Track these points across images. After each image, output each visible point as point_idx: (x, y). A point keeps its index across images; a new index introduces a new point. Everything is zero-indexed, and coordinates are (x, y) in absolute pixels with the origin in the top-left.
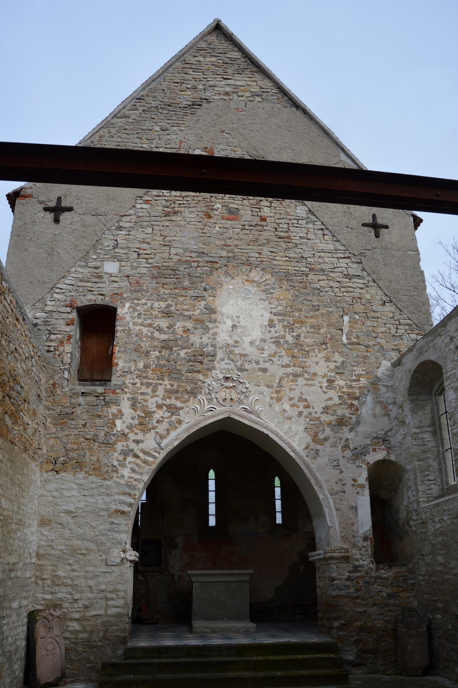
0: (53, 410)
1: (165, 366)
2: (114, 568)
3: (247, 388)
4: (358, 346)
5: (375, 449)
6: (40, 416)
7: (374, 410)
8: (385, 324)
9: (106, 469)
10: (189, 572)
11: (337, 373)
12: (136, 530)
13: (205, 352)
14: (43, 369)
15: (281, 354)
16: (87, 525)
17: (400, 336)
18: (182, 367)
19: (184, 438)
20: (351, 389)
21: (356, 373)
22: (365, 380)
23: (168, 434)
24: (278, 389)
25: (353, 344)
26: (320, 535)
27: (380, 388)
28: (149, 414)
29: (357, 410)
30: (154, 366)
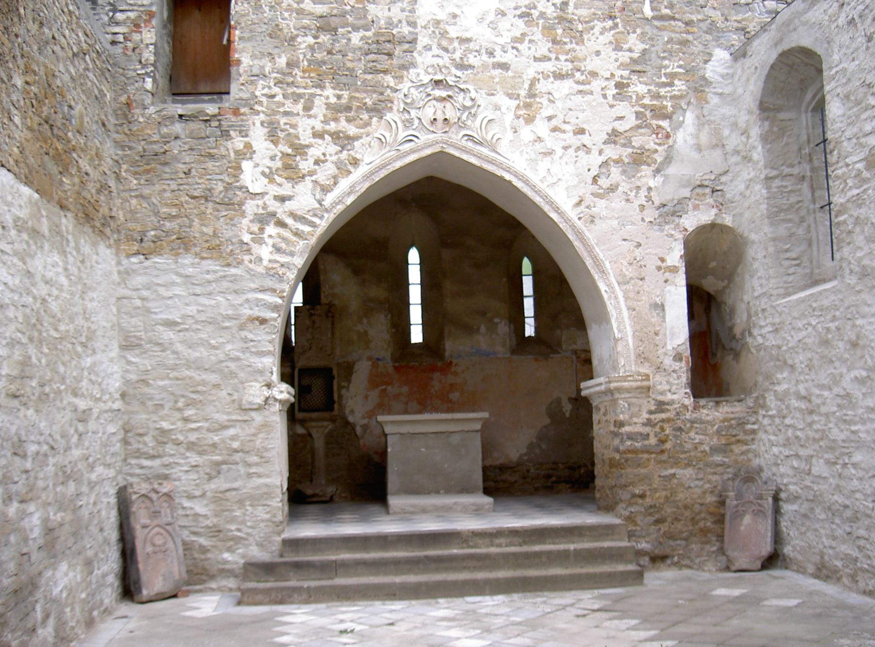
0: (130, 148)
1: (324, 63)
2: (254, 414)
3: (472, 100)
4: (672, 22)
5: (698, 205)
6: (109, 160)
7: (697, 136)
9: (231, 247)
10: (380, 418)
11: (634, 71)
12: (288, 353)
13: (397, 35)
14: (107, 75)
15: (533, 38)
16: (203, 345)
18: (355, 64)
19: (363, 190)
21: (668, 71)
23: (335, 184)
24: (528, 100)
25: (662, 18)
26: (599, 352)
28: (300, 150)
29: (668, 136)
30: (306, 63)
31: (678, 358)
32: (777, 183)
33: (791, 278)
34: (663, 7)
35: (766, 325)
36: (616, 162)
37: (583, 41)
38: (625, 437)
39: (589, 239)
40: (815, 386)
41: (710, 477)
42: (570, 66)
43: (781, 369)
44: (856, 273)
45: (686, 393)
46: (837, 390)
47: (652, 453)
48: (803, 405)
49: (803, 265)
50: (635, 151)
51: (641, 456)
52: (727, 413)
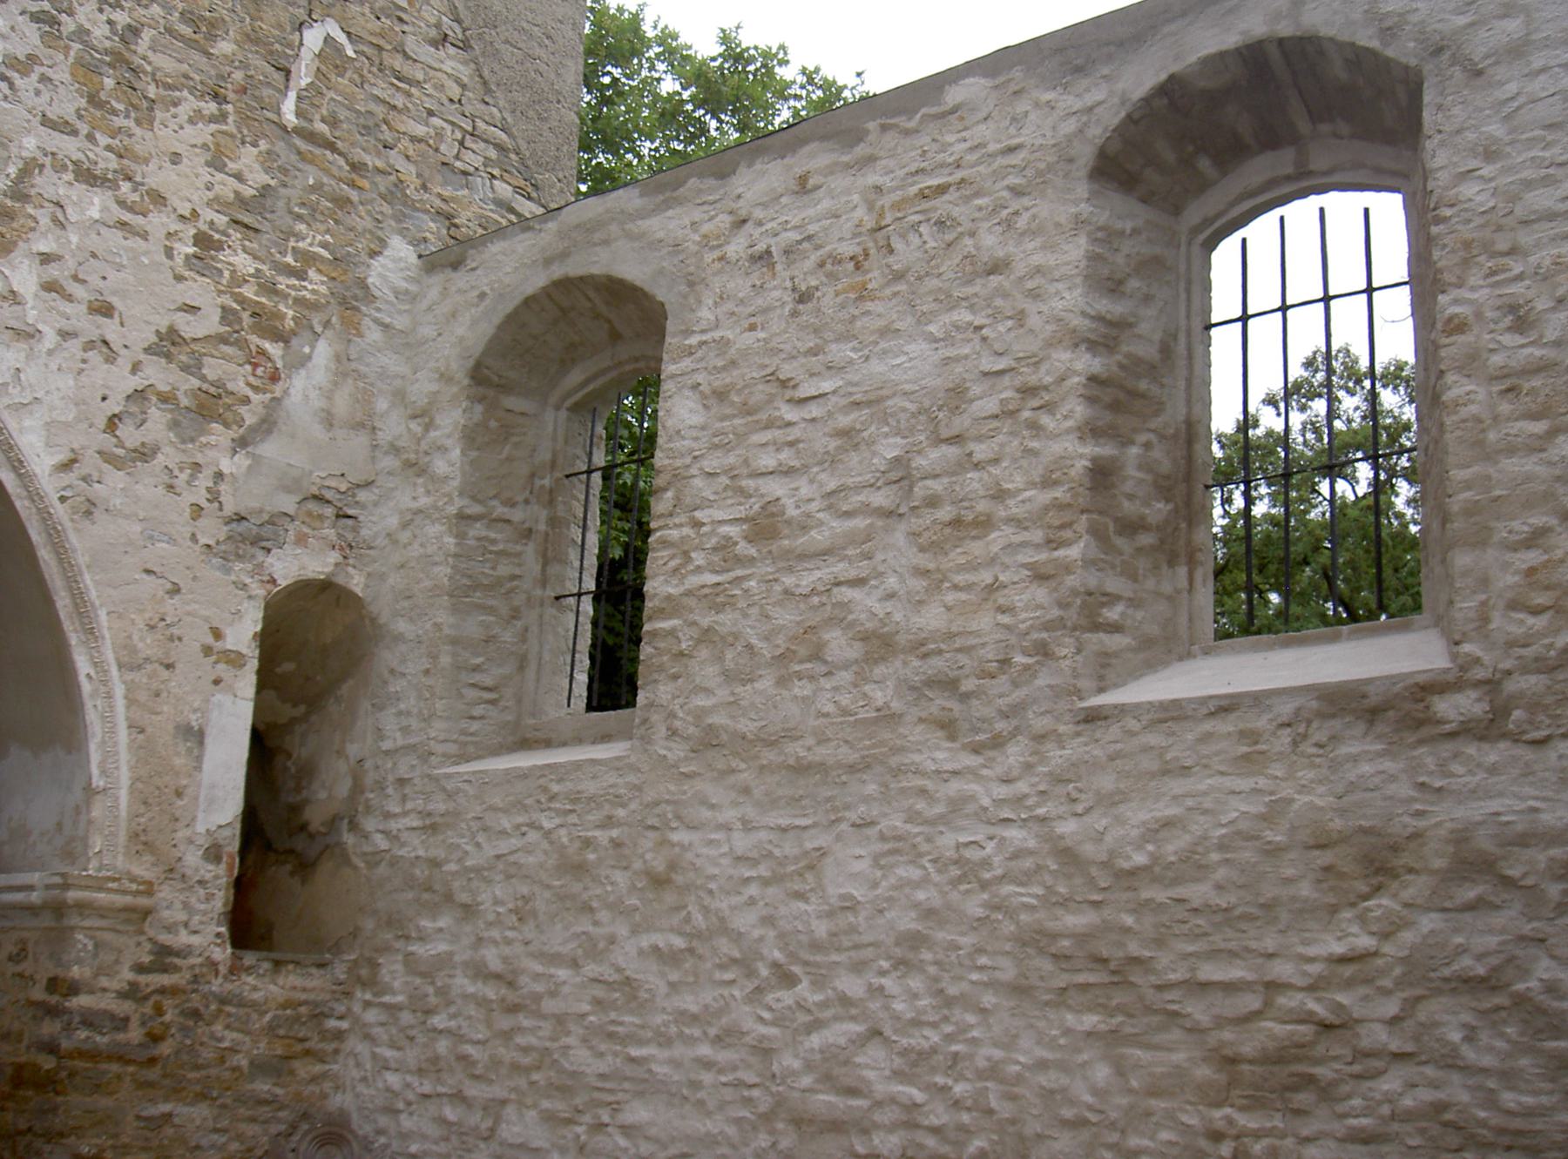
4: (328, 153)
5: (306, 535)
8: (431, 113)
11: (236, 222)
15: (50, 73)
17: (465, 173)
20: (270, 299)
21: (301, 244)
22: (323, 283)
24: (9, 203)
27: (363, 328)
29: (274, 378)
31: (213, 853)
32: (478, 529)
33: (475, 726)
34: (317, 117)
35: (405, 814)
36: (165, 398)
37: (151, 122)
38: (77, 1019)
39: (74, 551)
40: (533, 955)
41: (243, 1127)
42: (113, 162)
43: (434, 910)
44: (687, 739)
45: (218, 935)
46: (591, 969)
47: (129, 1062)
48: (491, 992)
49: (502, 703)
50: (205, 386)
51: (104, 1066)
52: (295, 988)
